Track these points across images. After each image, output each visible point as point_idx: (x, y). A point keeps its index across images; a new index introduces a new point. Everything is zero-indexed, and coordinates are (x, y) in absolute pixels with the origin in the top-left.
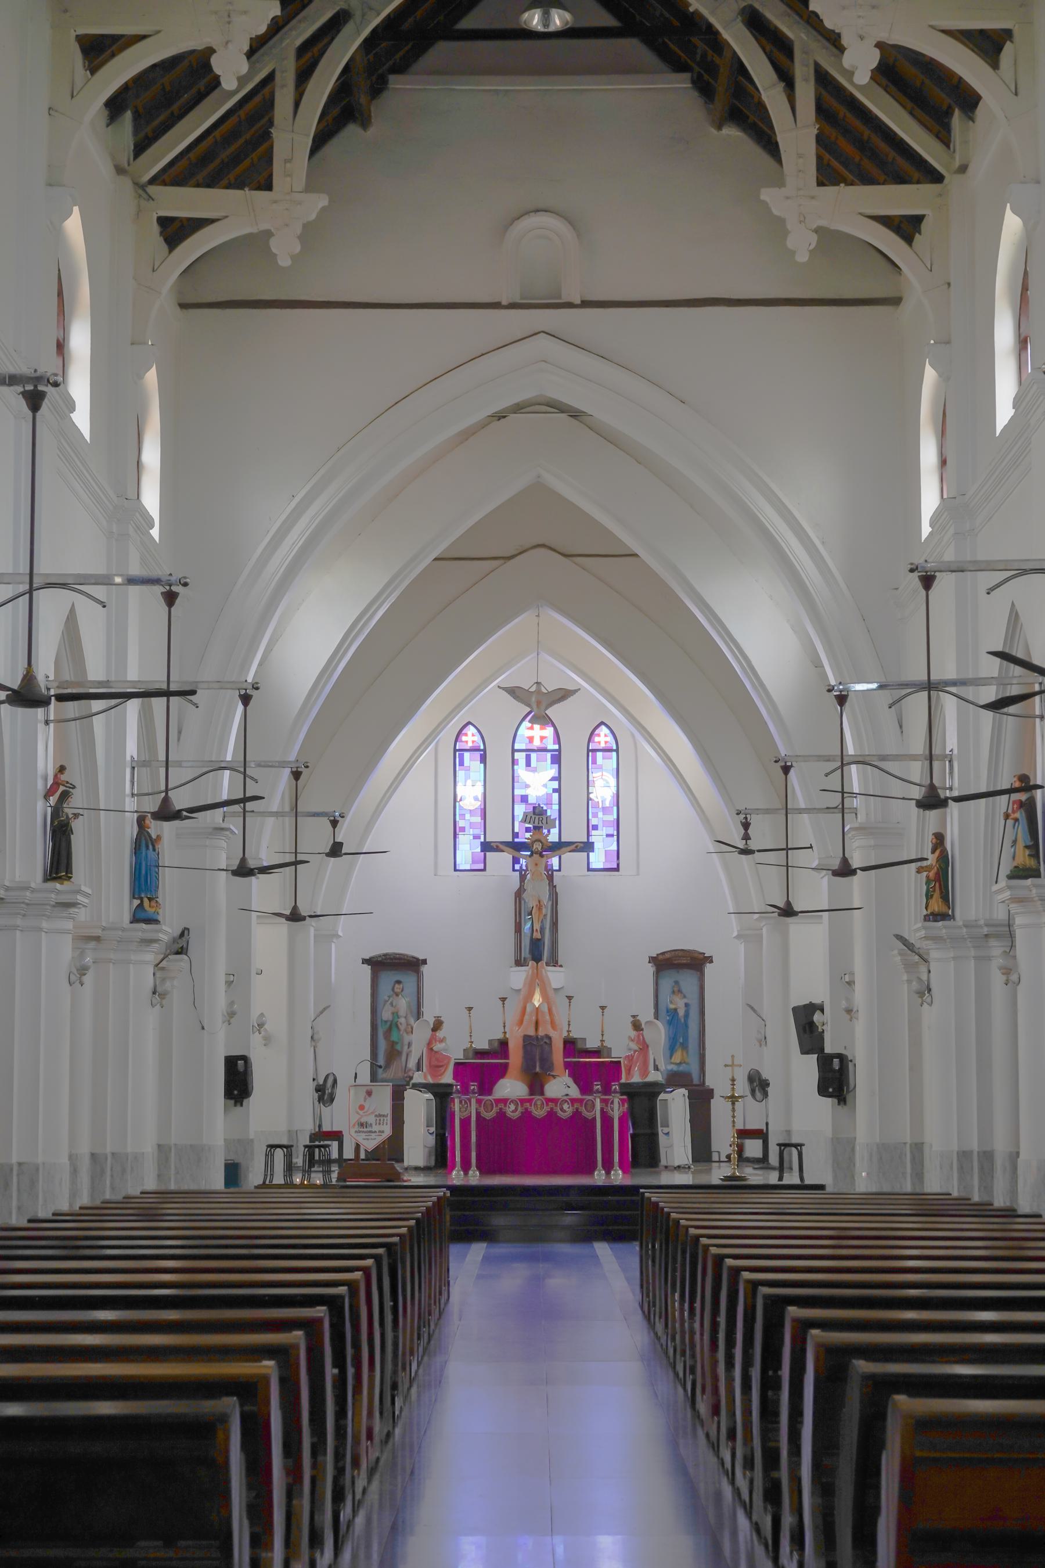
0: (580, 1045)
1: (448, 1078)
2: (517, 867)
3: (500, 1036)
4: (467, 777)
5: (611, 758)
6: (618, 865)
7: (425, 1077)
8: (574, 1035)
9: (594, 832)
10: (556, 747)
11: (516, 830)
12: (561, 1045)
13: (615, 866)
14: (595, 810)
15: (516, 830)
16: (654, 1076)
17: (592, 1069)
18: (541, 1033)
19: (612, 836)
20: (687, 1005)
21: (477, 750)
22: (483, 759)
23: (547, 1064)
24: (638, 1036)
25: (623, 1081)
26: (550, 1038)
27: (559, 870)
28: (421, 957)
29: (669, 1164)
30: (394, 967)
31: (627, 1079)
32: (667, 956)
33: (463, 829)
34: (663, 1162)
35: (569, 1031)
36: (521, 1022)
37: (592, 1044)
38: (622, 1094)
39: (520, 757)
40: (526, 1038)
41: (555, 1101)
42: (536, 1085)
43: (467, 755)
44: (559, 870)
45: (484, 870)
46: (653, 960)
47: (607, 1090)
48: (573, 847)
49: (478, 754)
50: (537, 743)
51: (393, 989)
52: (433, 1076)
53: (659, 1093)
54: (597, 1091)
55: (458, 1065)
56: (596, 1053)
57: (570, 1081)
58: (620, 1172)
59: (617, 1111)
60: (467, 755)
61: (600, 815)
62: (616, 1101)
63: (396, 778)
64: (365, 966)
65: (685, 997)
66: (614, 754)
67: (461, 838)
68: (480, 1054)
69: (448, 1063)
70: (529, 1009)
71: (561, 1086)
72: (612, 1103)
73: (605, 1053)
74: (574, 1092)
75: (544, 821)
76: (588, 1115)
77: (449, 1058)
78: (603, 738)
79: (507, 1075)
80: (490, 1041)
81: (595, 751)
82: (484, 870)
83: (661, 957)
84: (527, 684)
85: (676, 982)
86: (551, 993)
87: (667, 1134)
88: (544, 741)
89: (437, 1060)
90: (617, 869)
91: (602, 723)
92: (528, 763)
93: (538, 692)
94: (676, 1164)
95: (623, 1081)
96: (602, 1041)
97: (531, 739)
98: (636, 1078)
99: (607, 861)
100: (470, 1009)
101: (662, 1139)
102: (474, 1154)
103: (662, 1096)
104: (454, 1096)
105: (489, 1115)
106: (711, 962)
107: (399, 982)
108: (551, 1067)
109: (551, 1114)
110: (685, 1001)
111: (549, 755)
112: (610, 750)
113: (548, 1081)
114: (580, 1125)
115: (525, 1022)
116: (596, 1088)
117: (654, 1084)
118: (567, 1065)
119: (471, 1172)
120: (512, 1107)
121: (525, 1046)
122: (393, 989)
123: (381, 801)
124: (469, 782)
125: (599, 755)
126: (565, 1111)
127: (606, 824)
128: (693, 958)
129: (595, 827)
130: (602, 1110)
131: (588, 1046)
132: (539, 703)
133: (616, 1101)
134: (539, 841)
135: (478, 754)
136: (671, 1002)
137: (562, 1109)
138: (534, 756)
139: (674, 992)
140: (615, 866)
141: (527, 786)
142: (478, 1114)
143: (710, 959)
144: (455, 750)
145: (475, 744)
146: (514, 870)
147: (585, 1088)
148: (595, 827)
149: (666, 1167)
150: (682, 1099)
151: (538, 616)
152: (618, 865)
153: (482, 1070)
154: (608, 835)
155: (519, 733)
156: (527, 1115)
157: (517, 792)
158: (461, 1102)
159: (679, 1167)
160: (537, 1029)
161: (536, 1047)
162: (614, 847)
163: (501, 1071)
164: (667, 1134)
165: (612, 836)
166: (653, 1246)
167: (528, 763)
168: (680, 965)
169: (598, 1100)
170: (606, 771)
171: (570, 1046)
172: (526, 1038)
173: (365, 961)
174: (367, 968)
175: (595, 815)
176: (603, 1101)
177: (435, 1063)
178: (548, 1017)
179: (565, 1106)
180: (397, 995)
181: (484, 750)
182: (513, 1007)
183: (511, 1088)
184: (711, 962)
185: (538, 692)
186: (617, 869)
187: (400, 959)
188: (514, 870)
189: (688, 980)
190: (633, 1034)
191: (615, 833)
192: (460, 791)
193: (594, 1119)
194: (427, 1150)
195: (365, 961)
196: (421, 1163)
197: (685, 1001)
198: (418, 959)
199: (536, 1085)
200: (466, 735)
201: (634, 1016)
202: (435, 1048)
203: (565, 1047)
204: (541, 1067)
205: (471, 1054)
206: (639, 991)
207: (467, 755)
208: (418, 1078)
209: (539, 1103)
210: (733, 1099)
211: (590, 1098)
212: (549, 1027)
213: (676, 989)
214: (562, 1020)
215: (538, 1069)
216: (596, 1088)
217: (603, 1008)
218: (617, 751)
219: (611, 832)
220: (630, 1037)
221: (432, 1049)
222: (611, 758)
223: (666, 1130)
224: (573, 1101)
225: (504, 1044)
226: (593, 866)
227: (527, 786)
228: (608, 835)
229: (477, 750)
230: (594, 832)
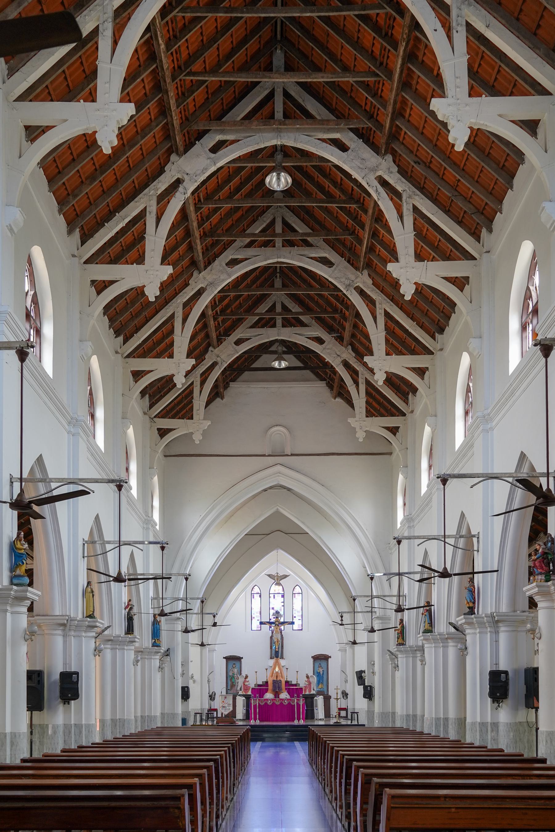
0: (290, 683)
1: (250, 693)
3: (266, 680)
8: (288, 680)
16: (313, 692)
17: (294, 690)
18: (278, 679)
22: (260, 596)
30: (233, 660)
34: (316, 718)
37: (294, 682)
41: (283, 700)
42: (277, 694)
46: (312, 657)
47: (298, 696)
56: (295, 685)
59: (301, 703)
67: (253, 620)
68: (259, 685)
71: (284, 695)
78: (298, 590)
84: (274, 573)
90: (302, 630)
93: (277, 576)
98: (307, 693)
101: (315, 711)
103: (315, 698)
105: (262, 704)
108: (281, 690)
109: (281, 703)
114: (290, 707)
117: (313, 694)
132: (277, 579)
143: (330, 657)
147: (292, 696)
148: (295, 617)
153: (261, 690)
156: (274, 703)
161: (277, 683)
163: (266, 691)
168: (321, 659)
171: (287, 683)
174: (225, 660)
183: (269, 696)
185: (277, 576)
186: (302, 630)
189: (323, 663)
190: (306, 679)
195: (224, 658)
196: (241, 718)
199: (277, 694)
214: (285, 674)
225: (267, 683)
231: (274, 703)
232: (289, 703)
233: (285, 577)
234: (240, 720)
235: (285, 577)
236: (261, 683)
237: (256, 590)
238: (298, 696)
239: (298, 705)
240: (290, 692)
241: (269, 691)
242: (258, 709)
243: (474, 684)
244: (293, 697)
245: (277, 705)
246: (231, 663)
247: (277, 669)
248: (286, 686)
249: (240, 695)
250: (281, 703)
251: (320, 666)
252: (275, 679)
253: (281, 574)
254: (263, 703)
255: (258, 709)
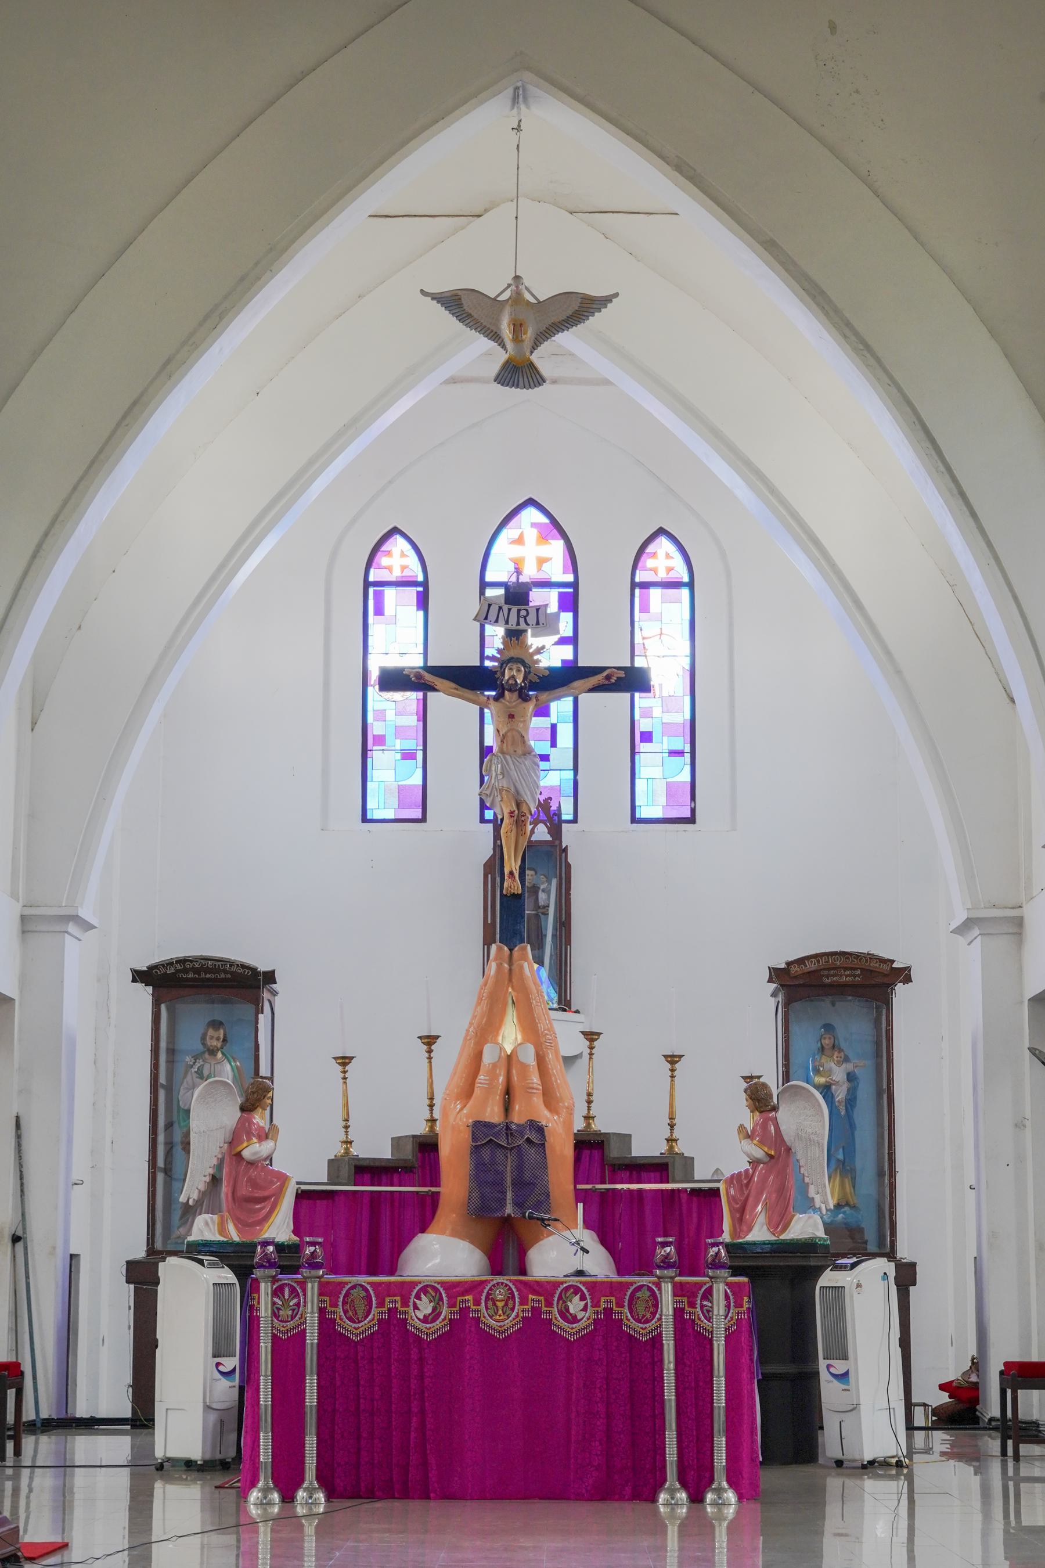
0: (614, 1152)
1: (280, 1228)
2: (489, 815)
3: (421, 1129)
5: (679, 601)
6: (693, 811)
7: (222, 1230)
8: (602, 1125)
9: (643, 747)
10: (570, 578)
11: (489, 741)
12: (569, 1152)
13: (688, 814)
15: (489, 741)
16: (806, 1226)
17: (646, 1206)
18: (518, 1117)
19: (680, 753)
20: (851, 1077)
21: (413, 583)
22: (423, 602)
23: (531, 1190)
24: (764, 1126)
25: (726, 1237)
26: (540, 1130)
27: (575, 821)
28: (262, 968)
29: (848, 1455)
30: (207, 995)
31: (735, 1233)
32: (811, 966)
33: (380, 740)
34: (830, 1445)
35: (588, 1118)
36: (467, 1091)
37: (646, 1146)
38: (736, 1271)
40: (480, 1128)
41: (547, 1289)
42: (505, 1244)
43: (390, 593)
44: (575, 821)
45: (423, 819)
46: (776, 975)
47: (690, 1261)
48: (594, 681)
49: (412, 593)
51: (203, 1038)
52: (242, 1224)
53: (819, 1271)
54: (666, 1264)
55: (303, 1197)
56: (659, 1168)
57: (589, 1238)
58: (731, 1496)
59: (720, 1317)
60: (390, 593)
62: (720, 1290)
63: (213, 579)
64: (140, 986)
65: (847, 1059)
66: (685, 592)
67: (378, 758)
68: (367, 1171)
69: (279, 1194)
70: (489, 1056)
71: (567, 1252)
72: (708, 1294)
73: (677, 1170)
74: (599, 1264)
75: (532, 619)
76: (641, 1330)
77: (283, 1178)
78: (664, 561)
79: (434, 1225)
80: (397, 1142)
81: (645, 586)
82: (423, 819)
83: (795, 969)
84: (493, 284)
85: (829, 1028)
86: (555, 1067)
87: (844, 1377)
88: (545, 567)
89: (254, 1184)
90: (691, 820)
91: (661, 531)
93: (517, 299)
94: (868, 1457)
95: (726, 1237)
96: (670, 1140)
98: (759, 1233)
100: (344, 1061)
101: (829, 1391)
102: (311, 1443)
103: (828, 1278)
104: (258, 1273)
105: (358, 1328)
106: (908, 979)
107: (216, 1024)
108: (544, 1202)
109: (535, 1325)
110: (850, 1067)
112: (676, 585)
113: (537, 1240)
114: (619, 1356)
115: (477, 1092)
116: (661, 1252)
117: (808, 1247)
118: (580, 1196)
119: (301, 1494)
120: (425, 1307)
121: (476, 1150)
122: (203, 1038)
123: (178, 630)
126: (575, 1320)
127: (668, 729)
128: (868, 972)
129: (647, 737)
130: (678, 1313)
131: (635, 1153)
132: (518, 327)
133: (720, 1290)
134: (522, 662)
135: (412, 593)
136: (817, 1071)
137: (564, 1314)
139: (822, 1049)
140: (688, 814)
142: (326, 1324)
143: (904, 975)
144: (367, 584)
145: (407, 573)
146: (483, 820)
147: (629, 1250)
148: (647, 737)
149: (839, 1463)
150: (881, 1285)
151: (518, 129)
152: (693, 811)
153: (371, 1208)
154: (673, 753)
155: (494, 551)
156: (463, 1324)
158: (277, 1292)
159: (872, 1463)
160: (507, 1108)
161: (506, 1154)
162: (685, 776)
163: (423, 1214)
164: (844, 1377)
165: (680, 753)
168: (839, 992)
169: (667, 1288)
171: (591, 1148)
172: (480, 1128)
173: (140, 976)
174: (144, 994)
176: (679, 1290)
177: (244, 1190)
178: (535, 1079)
179: (575, 1306)
180: (212, 1052)
181: (425, 584)
182: (450, 1055)
183: (443, 1255)
184: (908, 979)
185: (517, 299)
186: (691, 820)
187: (215, 970)
188: (483, 820)
189: (852, 1023)
190: (747, 1118)
191: (687, 748)
193: (656, 1341)
194: (213, 1417)
195: (140, 976)
196: (195, 1452)
197: (850, 1067)
198: (254, 970)
199: (505, 1244)
200: (389, 553)
201: (747, 1079)
202: (247, 1154)
203: (577, 1160)
204: (518, 1204)
205: (346, 1171)
206: (751, 1033)
207: (390, 594)
208: (204, 1228)
209: (500, 1294)
211: (644, 1280)
212: (538, 1101)
213: (826, 1042)
214: (572, 1085)
215: (509, 1210)
216: (661, 1252)
217: (673, 1060)
218: (691, 585)
219: (678, 747)
220: (741, 1128)
221: (239, 1155)
222: (679, 601)
223: (840, 1366)
224: (596, 1289)
225: (427, 1148)
226: (643, 813)
228: (673, 753)
229: (413, 583)
230: (643, 747)
231: (463, 1324)
232: (607, 1325)
233: (578, 309)
234: (189, 1464)
235: (578, 309)
236: (384, 1152)
237: (399, 560)
238: (690, 1261)
239: (693, 1342)
240: (607, 1220)
241: (449, 1211)
242: (311, 1384)
243: (312, 1368)
244: (646, 1266)
245: (486, 1338)
246: (195, 1018)
247: (510, 1035)
248: (579, 1176)
249: (196, 1251)
250: (535, 1325)
251: (830, 1046)
252: (493, 1114)
253: (542, 287)
254: (368, 1325)
255: (311, 1384)
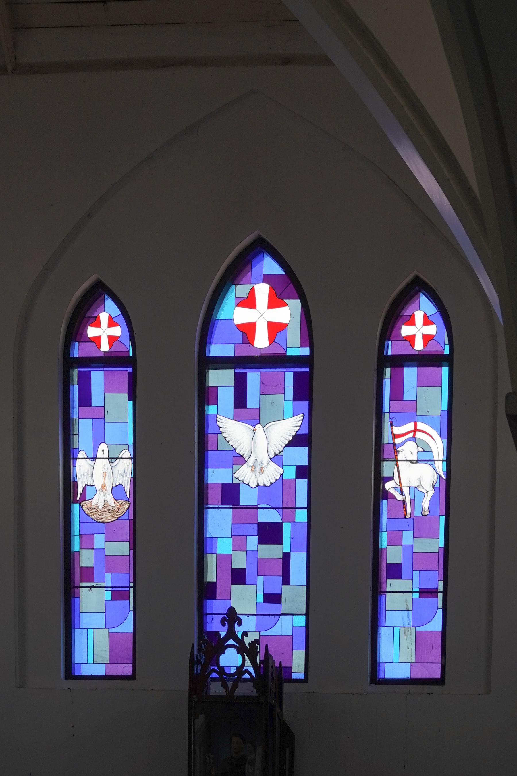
4: (99, 439)
10: (306, 351)
13: (437, 675)
14: (397, 525)
39: (221, 379)
43: (97, 377)
50: (261, 341)
61: (407, 537)
73: (397, 404)
81: (400, 362)
92: (240, 400)
97: (248, 331)
99: (418, 661)
111: (289, 377)
124: (103, 450)
125: (410, 374)
135: (122, 374)
138: (253, 378)
140: (437, 675)
141: (239, 460)
148: (395, 571)
154: (425, 593)
157: (216, 476)
166: (343, 460)
167: (240, 400)
170: (428, 419)
175: (396, 540)
192: (83, 471)
210: (103, 487)
219: (429, 586)
227: (239, 460)
228: (425, 593)
230: (391, 584)
